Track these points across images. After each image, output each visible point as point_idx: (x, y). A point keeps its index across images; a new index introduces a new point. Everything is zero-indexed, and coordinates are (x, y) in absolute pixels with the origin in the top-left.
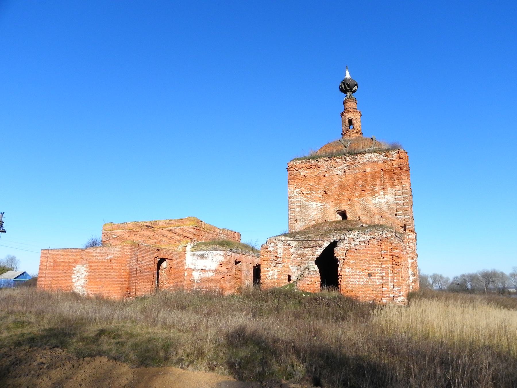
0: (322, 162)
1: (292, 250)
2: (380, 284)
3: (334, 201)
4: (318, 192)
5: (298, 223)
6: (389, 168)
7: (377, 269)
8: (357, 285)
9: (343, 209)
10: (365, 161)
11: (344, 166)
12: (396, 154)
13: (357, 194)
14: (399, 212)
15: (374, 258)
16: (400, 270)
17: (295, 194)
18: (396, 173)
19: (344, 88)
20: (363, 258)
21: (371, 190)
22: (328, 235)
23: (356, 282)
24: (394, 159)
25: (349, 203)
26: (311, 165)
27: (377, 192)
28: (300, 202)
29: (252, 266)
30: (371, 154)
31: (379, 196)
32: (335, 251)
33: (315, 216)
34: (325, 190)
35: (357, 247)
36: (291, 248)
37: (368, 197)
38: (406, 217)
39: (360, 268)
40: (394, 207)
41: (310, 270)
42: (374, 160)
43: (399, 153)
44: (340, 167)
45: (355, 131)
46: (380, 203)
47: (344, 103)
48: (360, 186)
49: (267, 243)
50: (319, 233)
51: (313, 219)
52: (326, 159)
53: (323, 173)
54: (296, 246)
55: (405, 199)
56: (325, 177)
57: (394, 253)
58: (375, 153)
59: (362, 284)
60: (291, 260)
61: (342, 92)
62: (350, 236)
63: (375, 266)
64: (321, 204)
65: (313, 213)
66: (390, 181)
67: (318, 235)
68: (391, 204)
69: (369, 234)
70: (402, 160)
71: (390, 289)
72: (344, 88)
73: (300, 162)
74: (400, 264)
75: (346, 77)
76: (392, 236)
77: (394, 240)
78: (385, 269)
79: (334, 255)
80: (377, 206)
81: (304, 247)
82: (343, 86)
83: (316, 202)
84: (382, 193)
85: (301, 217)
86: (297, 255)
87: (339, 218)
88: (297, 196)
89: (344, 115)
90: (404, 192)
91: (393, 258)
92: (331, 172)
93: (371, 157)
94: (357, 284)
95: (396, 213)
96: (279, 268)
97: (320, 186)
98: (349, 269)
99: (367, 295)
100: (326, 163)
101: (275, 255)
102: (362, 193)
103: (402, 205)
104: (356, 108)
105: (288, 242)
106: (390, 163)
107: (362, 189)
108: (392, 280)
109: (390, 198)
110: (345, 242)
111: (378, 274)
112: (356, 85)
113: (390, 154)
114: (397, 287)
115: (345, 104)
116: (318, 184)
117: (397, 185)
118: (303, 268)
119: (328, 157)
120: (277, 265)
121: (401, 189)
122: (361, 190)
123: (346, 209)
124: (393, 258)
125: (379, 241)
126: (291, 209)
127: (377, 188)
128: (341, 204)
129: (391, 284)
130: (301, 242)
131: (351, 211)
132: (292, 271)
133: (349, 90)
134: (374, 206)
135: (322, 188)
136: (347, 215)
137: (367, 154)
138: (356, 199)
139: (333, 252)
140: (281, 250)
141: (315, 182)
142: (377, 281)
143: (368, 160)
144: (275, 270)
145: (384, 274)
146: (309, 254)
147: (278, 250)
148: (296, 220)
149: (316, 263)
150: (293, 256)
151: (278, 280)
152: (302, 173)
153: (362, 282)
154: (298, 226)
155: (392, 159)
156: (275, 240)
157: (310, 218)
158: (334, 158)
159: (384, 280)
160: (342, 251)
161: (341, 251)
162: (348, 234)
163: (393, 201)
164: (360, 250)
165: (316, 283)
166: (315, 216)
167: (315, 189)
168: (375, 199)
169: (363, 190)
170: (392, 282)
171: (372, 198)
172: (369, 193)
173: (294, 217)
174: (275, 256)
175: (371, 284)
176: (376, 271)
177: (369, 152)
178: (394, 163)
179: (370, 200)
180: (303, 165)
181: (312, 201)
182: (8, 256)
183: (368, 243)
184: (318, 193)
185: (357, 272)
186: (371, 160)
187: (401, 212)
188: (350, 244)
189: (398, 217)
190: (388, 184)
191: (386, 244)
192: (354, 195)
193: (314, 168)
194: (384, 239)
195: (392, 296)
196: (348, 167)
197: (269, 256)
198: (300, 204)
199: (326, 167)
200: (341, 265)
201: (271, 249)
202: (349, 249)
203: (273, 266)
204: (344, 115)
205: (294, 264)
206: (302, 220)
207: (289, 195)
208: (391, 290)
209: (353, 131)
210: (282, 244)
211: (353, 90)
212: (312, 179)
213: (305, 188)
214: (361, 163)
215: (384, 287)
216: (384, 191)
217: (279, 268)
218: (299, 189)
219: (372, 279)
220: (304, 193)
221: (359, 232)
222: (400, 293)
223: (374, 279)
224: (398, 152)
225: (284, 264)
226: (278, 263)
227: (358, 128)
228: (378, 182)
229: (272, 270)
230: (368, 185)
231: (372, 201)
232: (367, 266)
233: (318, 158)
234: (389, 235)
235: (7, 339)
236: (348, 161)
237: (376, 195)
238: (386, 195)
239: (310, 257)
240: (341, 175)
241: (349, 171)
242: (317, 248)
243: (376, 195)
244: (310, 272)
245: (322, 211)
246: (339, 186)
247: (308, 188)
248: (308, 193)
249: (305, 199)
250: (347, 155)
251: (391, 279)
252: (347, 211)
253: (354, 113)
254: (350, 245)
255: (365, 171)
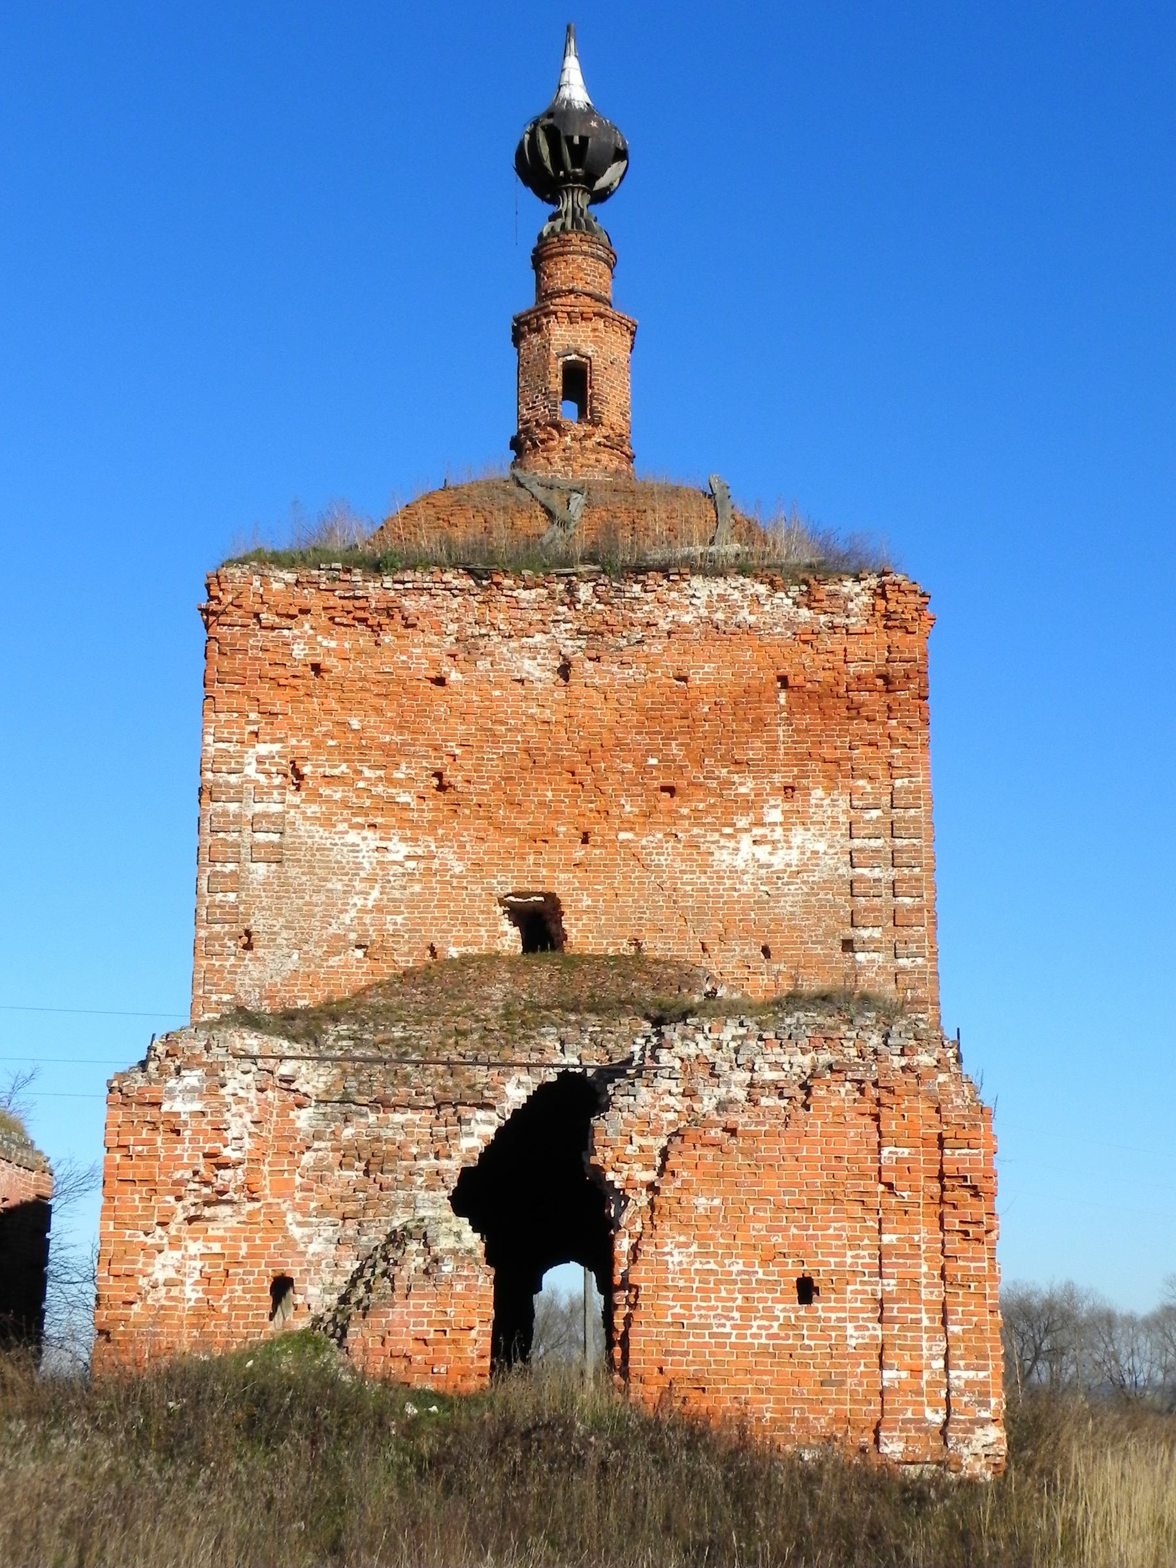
0: (425, 598)
1: (304, 1119)
2: (865, 1346)
3: (492, 833)
4: (398, 775)
5: (260, 952)
6: (821, 676)
7: (850, 1253)
8: (733, 1345)
9: (540, 888)
10: (687, 619)
11: (561, 633)
12: (865, 599)
13: (628, 808)
14: (865, 933)
15: (834, 1185)
16: (986, 1264)
17: (251, 770)
18: (863, 705)
19: (548, 164)
20: (770, 1183)
21: (710, 792)
22: (527, 1038)
23: (727, 1330)
24: (856, 623)
25: (579, 853)
26: (358, 604)
27: (749, 805)
28: (279, 824)
30: (721, 580)
31: (758, 831)
32: (599, 1138)
33: (367, 919)
34: (438, 765)
35: (739, 1120)
36: (300, 1106)
37: (695, 831)
38: (902, 962)
39: (755, 1247)
40: (840, 900)
41: (436, 1249)
42: (740, 618)
43: (883, 596)
44: (539, 638)
45: (597, 439)
46: (763, 872)
47: (539, 258)
48: (653, 761)
49: (152, 1066)
50: (468, 1024)
51: (353, 936)
52: (456, 582)
53: (435, 663)
54: (327, 1092)
55: (904, 858)
56: (440, 689)
57: (952, 1162)
58: (747, 580)
59: (763, 1341)
60: (298, 1180)
61: (527, 181)
62: (692, 1050)
63: (839, 1237)
64: (404, 849)
65: (358, 900)
66: (826, 752)
67: (463, 1034)
68: (826, 884)
69: (804, 1043)
70: (899, 634)
71: (926, 1375)
72: (548, 164)
73: (290, 577)
74: (987, 1232)
75: (565, 92)
76: (940, 1065)
77: (952, 1088)
78: (898, 1256)
79: (593, 1160)
80: (745, 889)
81: (382, 1104)
82: (545, 150)
83: (379, 834)
84: (775, 816)
85: (281, 920)
86: (334, 1150)
87: (510, 938)
88: (257, 786)
89: (538, 330)
90: (902, 819)
91: (948, 1195)
92: (483, 665)
93: (722, 598)
94: (733, 1339)
95: (849, 932)
96: (220, 1233)
97: (407, 737)
98: (687, 1245)
99: (787, 1411)
100: (455, 603)
101: (208, 1147)
102: (661, 806)
103: (886, 892)
104: (609, 295)
105: (286, 1069)
106: (830, 647)
107: (662, 781)
108: (938, 1324)
109: (821, 847)
110: (663, 1084)
111: (858, 1287)
112: (621, 155)
113: (833, 595)
114: (967, 1368)
115: (550, 267)
116: (400, 728)
117: (862, 777)
118: (374, 1236)
119: (471, 573)
120: (207, 1212)
121: (886, 799)
122: (656, 784)
123: (559, 891)
124: (948, 1195)
125: (868, 1086)
126: (218, 867)
127: (750, 784)
128: (531, 859)
129: (931, 1350)
130: (358, 1071)
131: (587, 901)
132: (303, 1253)
133: (577, 179)
134: (728, 883)
135: (422, 751)
136: (565, 925)
137: (697, 582)
138: (623, 836)
139: (583, 1139)
140: (248, 1118)
141: (379, 711)
142: (850, 1329)
143: (704, 612)
144: (189, 1243)
145: (891, 1285)
146: (414, 1150)
147: (227, 1116)
148: (248, 933)
149: (461, 1202)
150: (308, 1158)
151: (204, 1313)
152: (299, 650)
153: (759, 1332)
154: (255, 970)
155: (846, 627)
156: (208, 1048)
157: (333, 929)
158: (508, 582)
159: (892, 1321)
160: (642, 1134)
161: (636, 1138)
162: (676, 1036)
163: (833, 864)
164: (754, 1136)
165: (473, 1334)
166: (367, 919)
167: (376, 756)
168: (732, 844)
169: (664, 789)
170: (940, 1336)
171: (716, 836)
172: (701, 806)
173: (232, 914)
174: (206, 1156)
175: (812, 1343)
176: (843, 1264)
177: (713, 569)
178: (856, 649)
179: (703, 848)
180: (309, 597)
181: (353, 826)
183: (801, 1096)
184: (391, 782)
185: (735, 1268)
186: (719, 616)
187: (877, 933)
188: (691, 1094)
189: (860, 957)
190: (811, 765)
191: (908, 1109)
192: (614, 811)
193: (377, 629)
194: (897, 1080)
195: (936, 1417)
196: (583, 643)
197: (162, 1153)
198: (275, 838)
199: (453, 627)
200: (632, 1222)
201: (180, 1106)
202: (682, 1124)
203: (180, 1216)
204: (538, 330)
205: (313, 1205)
206: (285, 934)
207: (209, 775)
208: (929, 1383)
209: (588, 436)
210: (250, 1077)
211: (601, 183)
212: (362, 689)
213: (317, 745)
214: (664, 625)
215: (891, 1367)
216: (787, 806)
217: (214, 1230)
218: (277, 747)
219: (820, 1313)
220: (306, 770)
221: (742, 1031)
222: (986, 1405)
223: (833, 1316)
224: (882, 586)
225: (257, 1205)
226: (219, 1198)
227: (614, 419)
228: (755, 750)
229: (175, 1243)
230: (700, 763)
231: (717, 855)
232: (794, 1231)
233: (404, 569)
234: (925, 1059)
236: (586, 604)
237: (740, 825)
238: (800, 828)
239: (422, 1163)
240: (539, 685)
241: (589, 665)
242: (466, 1112)
243: (742, 822)
244: (436, 1261)
245: (417, 888)
246: (527, 751)
247: (331, 743)
248: (336, 772)
249: (313, 809)
250: (582, 569)
251: (932, 1320)
252: (565, 901)
253: (600, 324)
254: (688, 1101)
255: (684, 679)
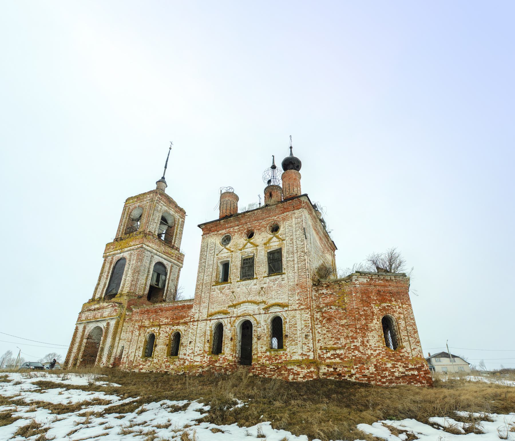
29: (238, 323)
182: (494, 370)
211: (272, 255)
235: (181, 220)
